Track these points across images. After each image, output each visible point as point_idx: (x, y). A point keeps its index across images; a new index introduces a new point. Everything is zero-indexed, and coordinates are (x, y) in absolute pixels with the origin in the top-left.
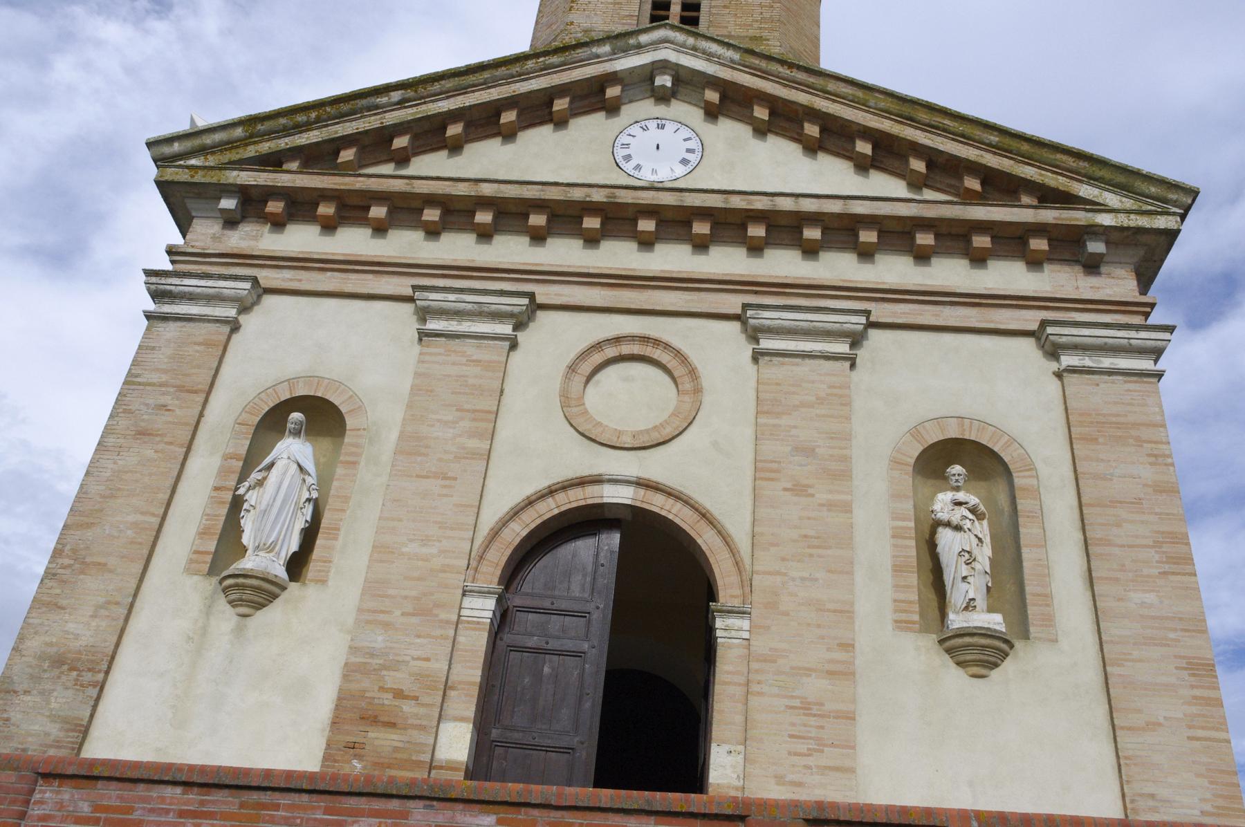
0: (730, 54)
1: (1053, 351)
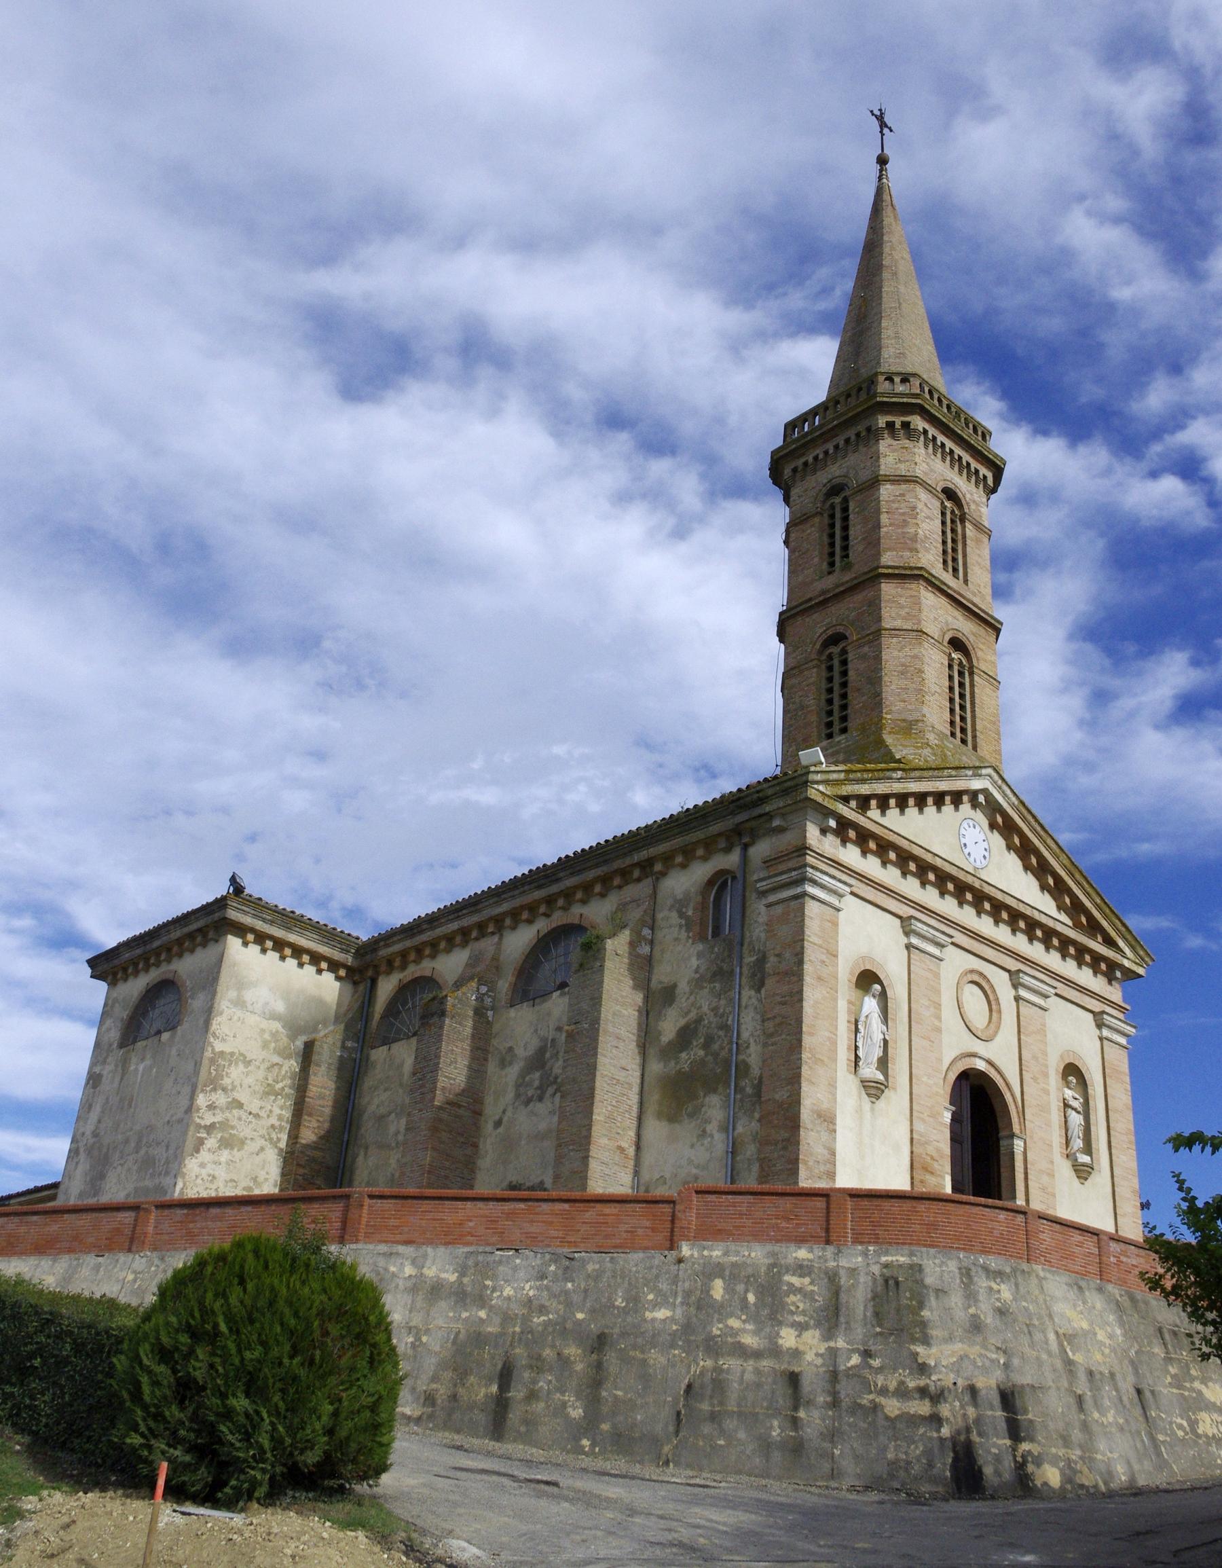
0: (1014, 799)
1: (1100, 1025)
